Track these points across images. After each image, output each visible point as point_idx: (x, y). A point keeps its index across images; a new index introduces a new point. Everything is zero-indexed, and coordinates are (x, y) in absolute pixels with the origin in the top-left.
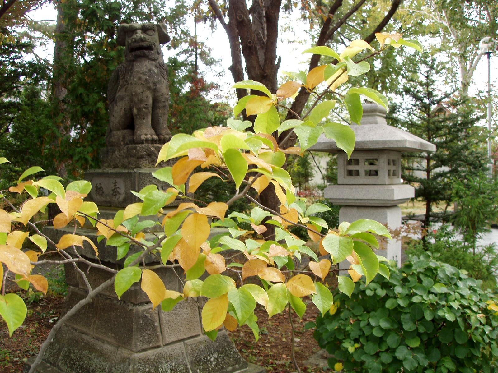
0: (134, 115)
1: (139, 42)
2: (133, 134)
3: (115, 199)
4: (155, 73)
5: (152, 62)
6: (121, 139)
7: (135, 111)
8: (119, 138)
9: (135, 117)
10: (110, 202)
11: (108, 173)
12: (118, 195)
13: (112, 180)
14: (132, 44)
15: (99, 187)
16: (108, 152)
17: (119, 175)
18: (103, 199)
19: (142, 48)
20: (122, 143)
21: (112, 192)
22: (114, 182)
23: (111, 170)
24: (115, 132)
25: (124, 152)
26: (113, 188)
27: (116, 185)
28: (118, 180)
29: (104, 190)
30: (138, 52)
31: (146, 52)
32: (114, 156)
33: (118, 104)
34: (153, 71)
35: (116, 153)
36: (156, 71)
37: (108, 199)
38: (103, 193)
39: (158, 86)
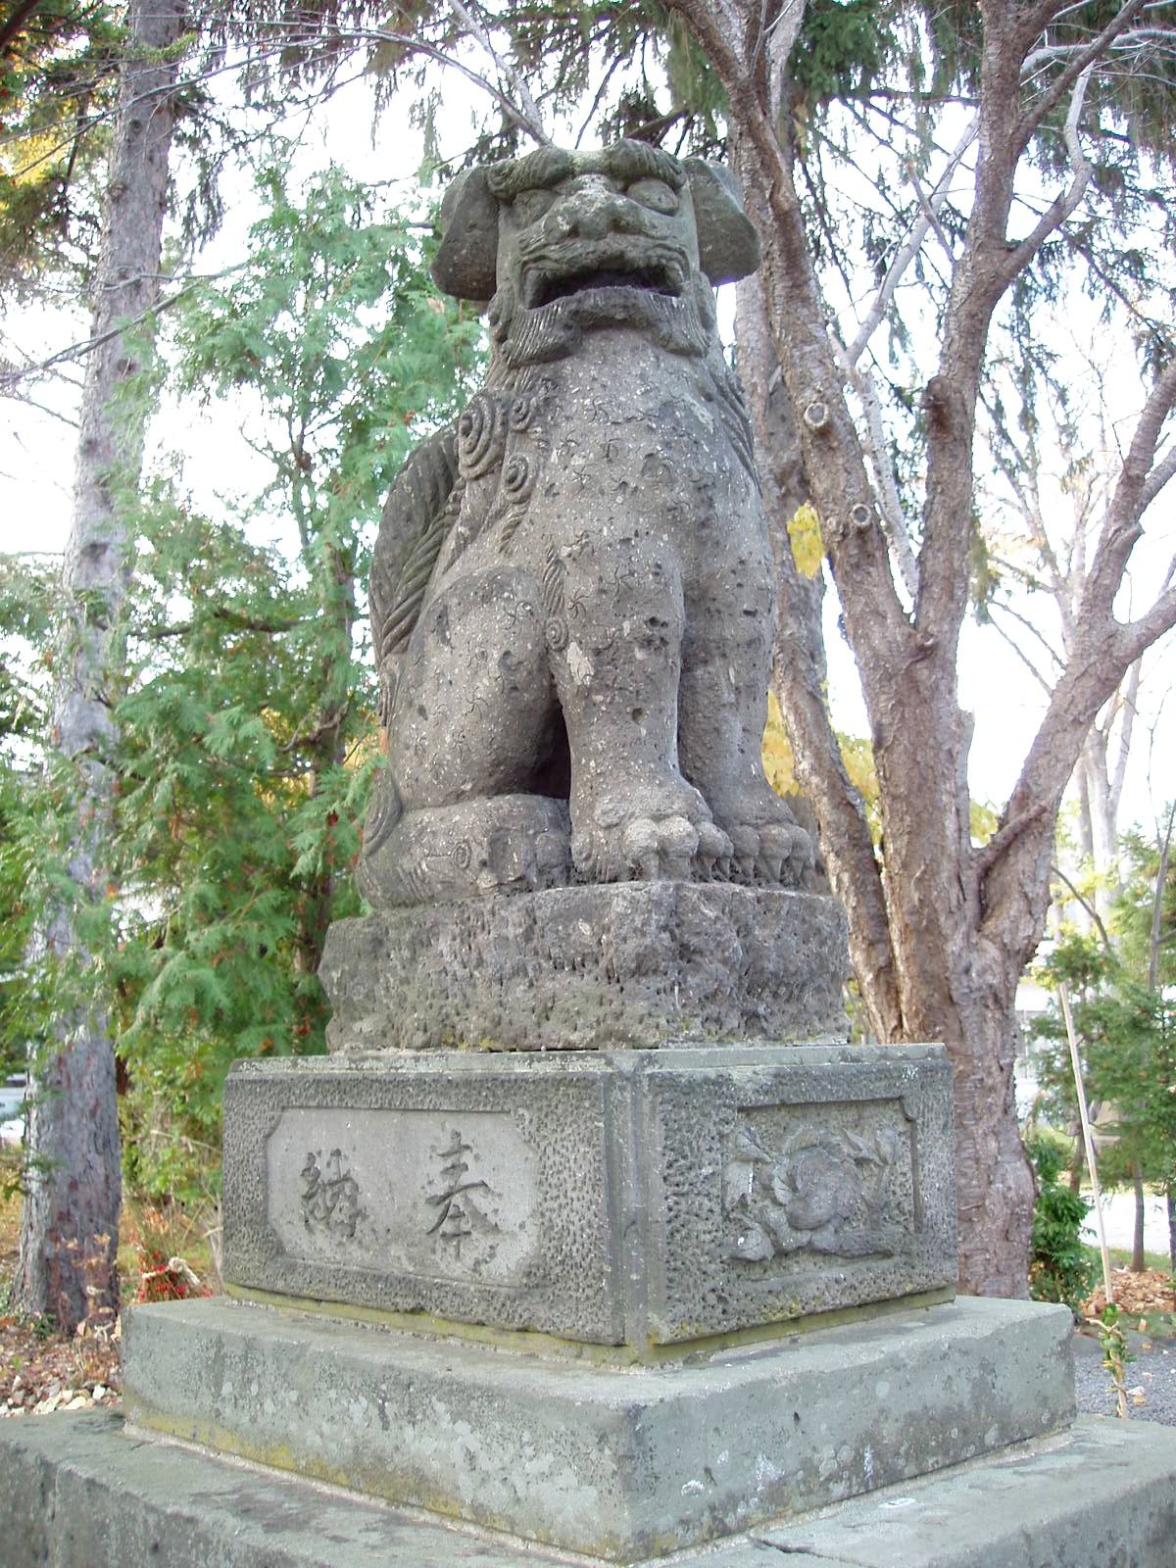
0: (566, 692)
1: (600, 236)
2: (563, 823)
3: (452, 1266)
4: (702, 427)
5: (676, 362)
6: (480, 853)
7: (577, 664)
8: (462, 852)
9: (572, 712)
10: (407, 1284)
11: (399, 1084)
12: (480, 1243)
13: (432, 1131)
14: (553, 252)
15: (328, 1174)
16: (378, 942)
17: (485, 1095)
18: (357, 1256)
19: (613, 271)
20: (486, 880)
21: (428, 1216)
22: (446, 1144)
23: (405, 1061)
24: (427, 816)
25: (502, 941)
26: (440, 1188)
27: (456, 1169)
28: (479, 1130)
29: (367, 1197)
30: (593, 298)
31: (644, 296)
32: (426, 965)
33: (457, 630)
34: (688, 410)
35: (443, 945)
36: (704, 414)
37: (399, 1260)
38: (359, 1214)
39: (719, 507)
